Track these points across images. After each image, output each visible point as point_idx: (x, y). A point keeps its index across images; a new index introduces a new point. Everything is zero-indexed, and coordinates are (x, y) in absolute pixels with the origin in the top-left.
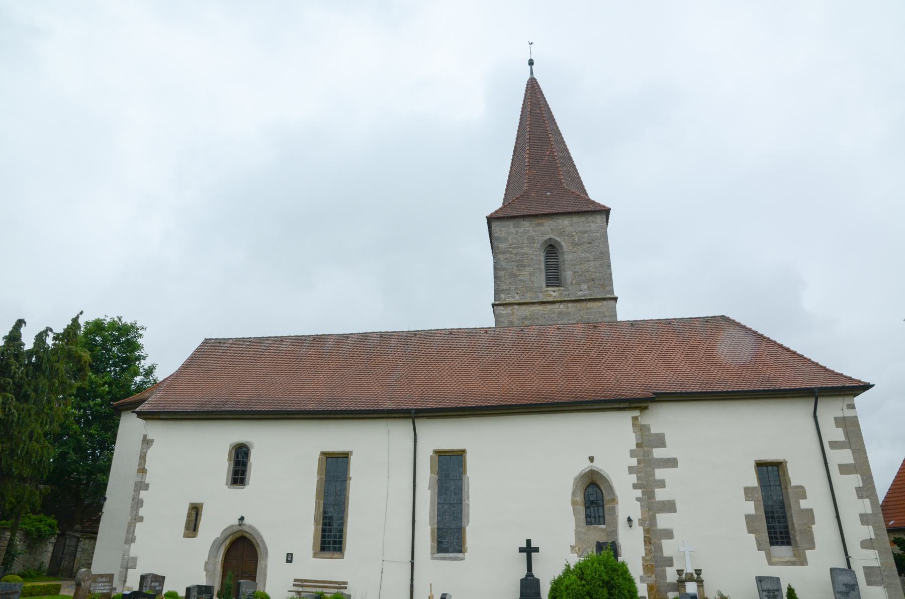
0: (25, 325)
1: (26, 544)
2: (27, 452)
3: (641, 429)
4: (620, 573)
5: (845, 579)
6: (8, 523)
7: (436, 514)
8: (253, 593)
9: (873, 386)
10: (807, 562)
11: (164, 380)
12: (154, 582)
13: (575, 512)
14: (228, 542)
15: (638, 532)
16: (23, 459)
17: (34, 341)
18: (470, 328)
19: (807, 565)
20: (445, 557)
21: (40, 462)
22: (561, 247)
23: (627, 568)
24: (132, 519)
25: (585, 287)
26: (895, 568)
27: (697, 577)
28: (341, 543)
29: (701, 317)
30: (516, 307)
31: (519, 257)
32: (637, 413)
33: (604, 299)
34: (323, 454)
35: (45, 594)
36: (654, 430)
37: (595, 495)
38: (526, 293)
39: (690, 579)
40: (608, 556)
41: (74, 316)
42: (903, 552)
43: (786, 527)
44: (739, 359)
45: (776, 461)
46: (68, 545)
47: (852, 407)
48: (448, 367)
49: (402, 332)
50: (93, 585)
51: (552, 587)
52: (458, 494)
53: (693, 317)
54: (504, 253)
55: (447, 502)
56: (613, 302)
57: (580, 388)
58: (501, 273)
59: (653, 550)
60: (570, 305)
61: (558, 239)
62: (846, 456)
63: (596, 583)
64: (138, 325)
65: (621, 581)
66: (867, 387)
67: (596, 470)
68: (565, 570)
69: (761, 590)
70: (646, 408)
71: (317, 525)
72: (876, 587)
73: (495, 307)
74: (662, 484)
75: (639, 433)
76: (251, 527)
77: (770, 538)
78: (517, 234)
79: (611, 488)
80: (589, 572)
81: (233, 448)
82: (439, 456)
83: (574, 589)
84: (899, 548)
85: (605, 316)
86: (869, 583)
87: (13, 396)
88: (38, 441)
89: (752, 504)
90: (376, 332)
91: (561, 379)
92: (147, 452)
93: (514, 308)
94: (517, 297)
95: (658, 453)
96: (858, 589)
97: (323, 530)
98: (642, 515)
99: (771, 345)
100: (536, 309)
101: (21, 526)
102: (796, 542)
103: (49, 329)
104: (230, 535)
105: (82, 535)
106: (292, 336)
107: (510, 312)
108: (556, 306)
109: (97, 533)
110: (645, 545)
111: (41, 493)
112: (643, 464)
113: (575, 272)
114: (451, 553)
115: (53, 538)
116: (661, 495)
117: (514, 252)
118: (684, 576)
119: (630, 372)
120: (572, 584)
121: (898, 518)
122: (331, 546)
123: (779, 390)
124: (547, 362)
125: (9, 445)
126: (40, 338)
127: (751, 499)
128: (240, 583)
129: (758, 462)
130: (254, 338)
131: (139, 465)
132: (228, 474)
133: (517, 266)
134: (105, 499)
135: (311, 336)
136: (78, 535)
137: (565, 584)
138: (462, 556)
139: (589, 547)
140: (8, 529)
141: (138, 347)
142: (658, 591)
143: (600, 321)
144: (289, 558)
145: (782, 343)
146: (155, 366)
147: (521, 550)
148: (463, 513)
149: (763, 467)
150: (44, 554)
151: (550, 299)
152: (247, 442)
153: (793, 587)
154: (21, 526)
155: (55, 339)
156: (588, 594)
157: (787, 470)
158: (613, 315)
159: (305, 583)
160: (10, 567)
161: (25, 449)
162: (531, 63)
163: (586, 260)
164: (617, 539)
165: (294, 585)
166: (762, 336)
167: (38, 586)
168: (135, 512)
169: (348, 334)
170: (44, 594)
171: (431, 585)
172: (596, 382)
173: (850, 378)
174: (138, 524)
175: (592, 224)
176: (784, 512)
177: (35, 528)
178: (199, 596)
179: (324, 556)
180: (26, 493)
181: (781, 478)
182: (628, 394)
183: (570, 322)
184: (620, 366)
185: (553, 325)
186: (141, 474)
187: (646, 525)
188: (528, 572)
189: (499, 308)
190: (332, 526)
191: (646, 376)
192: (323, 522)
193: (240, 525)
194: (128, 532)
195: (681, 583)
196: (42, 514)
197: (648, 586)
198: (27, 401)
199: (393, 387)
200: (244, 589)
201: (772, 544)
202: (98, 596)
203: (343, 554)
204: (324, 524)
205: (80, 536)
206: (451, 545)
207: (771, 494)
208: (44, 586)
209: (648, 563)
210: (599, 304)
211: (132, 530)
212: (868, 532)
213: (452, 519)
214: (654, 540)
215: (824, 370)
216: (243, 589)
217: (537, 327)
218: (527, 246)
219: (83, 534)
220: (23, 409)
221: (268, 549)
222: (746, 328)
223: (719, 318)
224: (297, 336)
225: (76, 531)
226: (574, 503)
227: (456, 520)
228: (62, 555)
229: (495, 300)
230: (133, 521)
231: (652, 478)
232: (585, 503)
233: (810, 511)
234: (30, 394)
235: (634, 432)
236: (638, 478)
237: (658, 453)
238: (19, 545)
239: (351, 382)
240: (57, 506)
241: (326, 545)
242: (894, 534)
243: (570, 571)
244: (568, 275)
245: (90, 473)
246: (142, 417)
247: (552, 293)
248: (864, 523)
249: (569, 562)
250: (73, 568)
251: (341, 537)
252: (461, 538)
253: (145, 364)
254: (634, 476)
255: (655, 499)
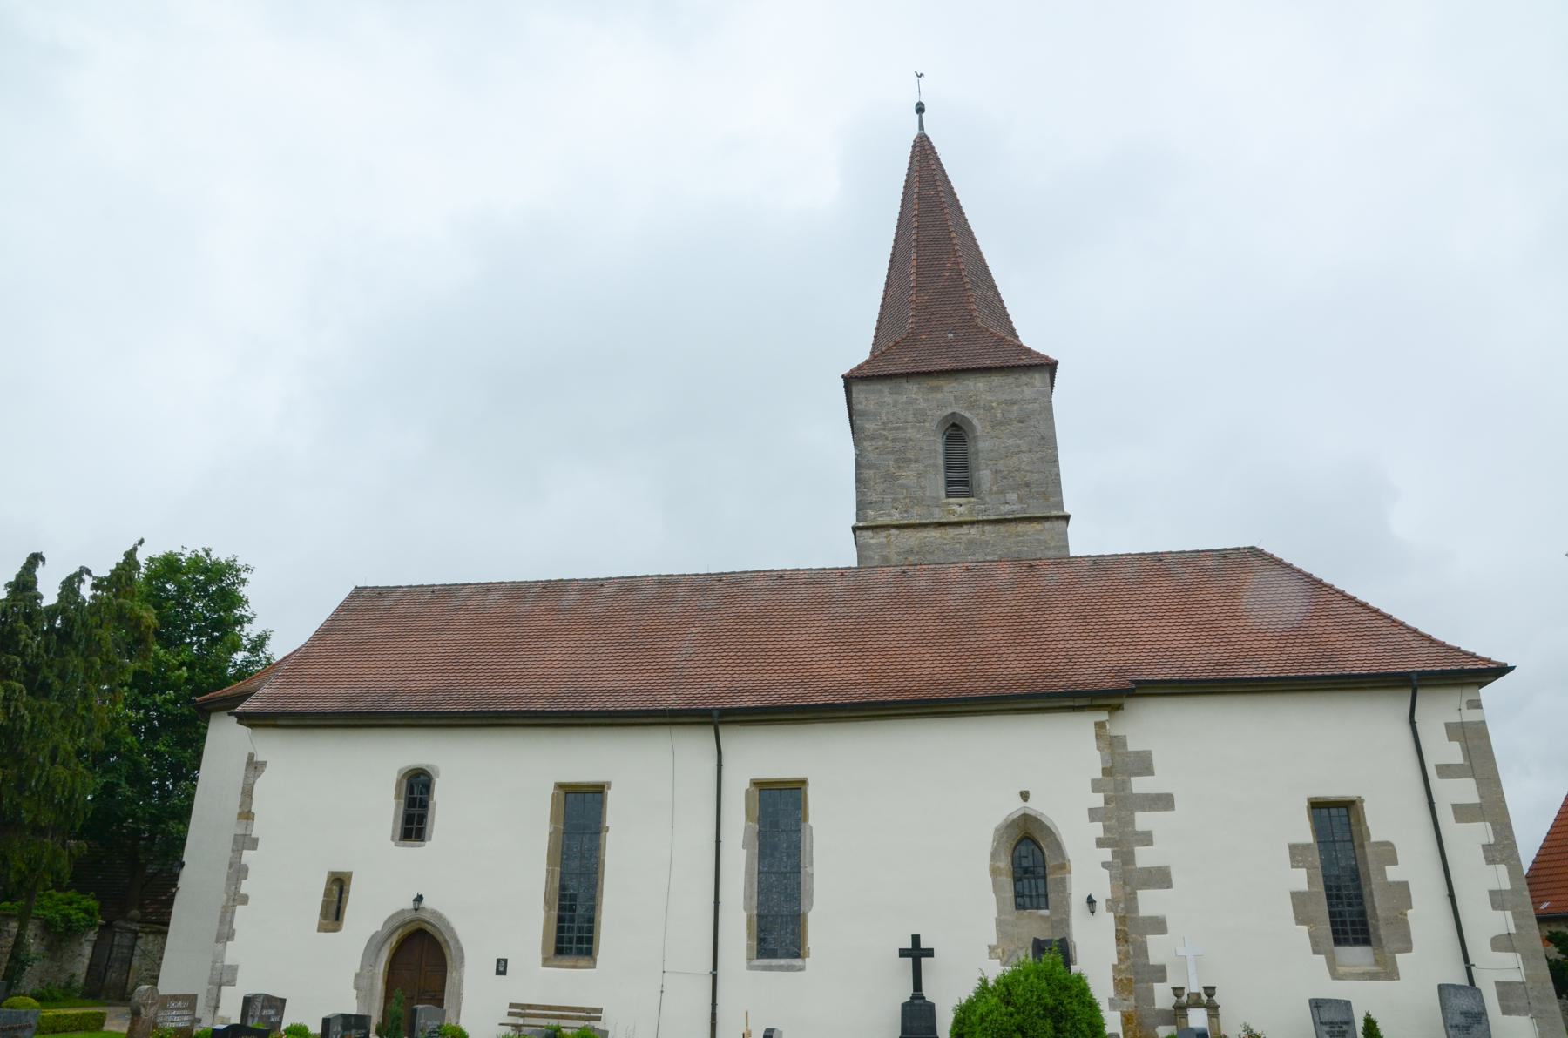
0: (44, 564)
1: (45, 943)
2: (47, 784)
3: (1110, 744)
4: (1074, 992)
5: (1465, 1003)
6: (14, 906)
7: (756, 890)
8: (439, 1027)
9: (1512, 668)
10: (1398, 975)
11: (285, 658)
12: (267, 1009)
13: (997, 888)
14: (394, 939)
15: (1106, 922)
16: (40, 796)
17: (60, 591)
18: (814, 568)
19: (1399, 979)
20: (771, 966)
21: (69, 800)
22: (973, 428)
23: (1086, 985)
24: (228, 900)
25: (1013, 497)
26: (1551, 984)
27: (1208, 1000)
28: (590, 940)
29: (1214, 549)
30: (894, 531)
31: (899, 445)
32: (1103, 716)
33: (1047, 518)
34: (560, 786)
35: (78, 1029)
36: (1133, 745)
37: (1030, 858)
38: (912, 507)
39: (1196, 1002)
40: (1053, 964)
41: (129, 547)
42: (1564, 956)
43: (1363, 913)
44: (1280, 623)
45: (1344, 799)
46: (119, 945)
47: (1476, 705)
48: (776, 636)
49: (697, 575)
50: (161, 1013)
51: (956, 1017)
52: (794, 856)
53: (1200, 549)
54: (873, 438)
55: (775, 870)
56: (1062, 523)
57: (1005, 673)
58: (868, 474)
59: (1131, 952)
60: (987, 528)
61: (967, 414)
62: (1465, 791)
63: (1032, 1010)
64: (240, 563)
65: (1075, 1006)
66: (1502, 670)
67: (1033, 814)
68: (978, 988)
69: (1318, 1023)
70: (1119, 707)
71: (550, 910)
72: (1518, 1017)
73: (858, 533)
74: (1146, 839)
75: (1107, 751)
76: (434, 913)
77: (1335, 932)
78: (895, 405)
79: (1058, 846)
80: (1020, 991)
81: (403, 776)
82: (760, 790)
83: (995, 1021)
84: (1557, 950)
85: (1048, 548)
86: (1506, 1010)
87: (22, 686)
88: (65, 765)
89: (1302, 873)
90: (652, 576)
91: (973, 657)
92: (254, 783)
93: (890, 535)
94: (896, 515)
95: (1140, 785)
96: (1487, 1020)
97: (560, 919)
98: (1112, 893)
99: (1336, 599)
100: (928, 535)
101: (36, 911)
102: (1380, 940)
103: (85, 571)
104: (398, 927)
105: (142, 928)
106: (506, 583)
107: (884, 540)
108: (964, 530)
109: (167, 924)
110: (1118, 945)
111: (71, 854)
112: (1114, 805)
113: (996, 471)
114: (781, 958)
115: (92, 933)
116: (1144, 857)
117: (890, 437)
118: (1185, 999)
119: (1092, 645)
120: (992, 1012)
121: (1556, 898)
122: (574, 945)
123: (1350, 676)
124: (948, 627)
125: (16, 770)
126: (70, 586)
127: (1300, 864)
128: (416, 1010)
129: (1314, 801)
130: (441, 585)
131: (240, 806)
132: (395, 822)
133: (896, 461)
134: (182, 865)
135: (538, 582)
136: (136, 927)
137: (978, 1012)
138: (801, 963)
139: (1021, 949)
140: (14, 916)
141: (239, 601)
142: (1140, 1024)
143: (1039, 556)
144: (501, 967)
145: (1354, 595)
146: (268, 634)
147: (903, 953)
148: (802, 888)
149: (1322, 810)
150: (77, 960)
151: (954, 518)
152: (427, 766)
153: (1373, 1017)
154: (36, 911)
155: (95, 587)
156: (1018, 1029)
157: (1364, 814)
158: (1063, 547)
159: (528, 1011)
160: (18, 983)
161: (44, 779)
162: (920, 109)
163: (1016, 450)
164: (1068, 934)
165: (510, 1014)
166: (1320, 582)
167: (66, 1015)
168: (234, 887)
169: (602, 579)
170: (77, 1030)
171: (747, 1013)
172: (1032, 661)
173: (1473, 656)
174: (240, 909)
175: (1025, 388)
176: (1359, 887)
177: (61, 914)
178: (346, 1033)
179: (562, 964)
180: (45, 854)
181: (1353, 828)
182: (1089, 683)
183: (988, 558)
184: (1075, 634)
185: (958, 563)
186: (245, 821)
187: (1119, 909)
188: (914, 991)
189: (865, 533)
190: (575, 911)
191: (1120, 651)
192: (559, 905)
193: (416, 910)
194: (221, 922)
195: (1180, 1011)
196: (73, 890)
197: (1122, 1015)
198: (46, 696)
199: (680, 670)
200: (422, 1021)
201: (1337, 942)
202: (170, 1033)
203: (595, 961)
204: (561, 908)
205: (138, 929)
206: (781, 944)
207: (1336, 856)
208: (77, 1016)
209: (1122, 976)
210: (1037, 526)
211: (228, 919)
212: (1504, 922)
213: (782, 899)
214: (1134, 936)
215: (1427, 642)
216: (421, 1021)
217: (930, 567)
218: (913, 427)
219: (144, 925)
220: (40, 709)
221: (465, 951)
222: (1293, 569)
223: (1246, 551)
224: (514, 582)
225: (132, 920)
226: (994, 872)
227: (790, 901)
228: (108, 962)
229: (858, 520)
230: (231, 903)
231: (1130, 829)
232: (1014, 872)
233: (1404, 886)
234: (52, 683)
235: (1098, 749)
236: (1106, 829)
237: (1140, 785)
238: (33, 944)
239: (608, 662)
240: (99, 877)
241: (565, 945)
242: (1549, 926)
243: (987, 989)
244: (984, 476)
245: (156, 820)
246: (246, 723)
247: (956, 508)
248: (1496, 906)
249: (986, 975)
250: (127, 984)
251: (591, 930)
252: (799, 931)
253: (251, 631)
254: (1099, 826)
255: (1134, 864)
